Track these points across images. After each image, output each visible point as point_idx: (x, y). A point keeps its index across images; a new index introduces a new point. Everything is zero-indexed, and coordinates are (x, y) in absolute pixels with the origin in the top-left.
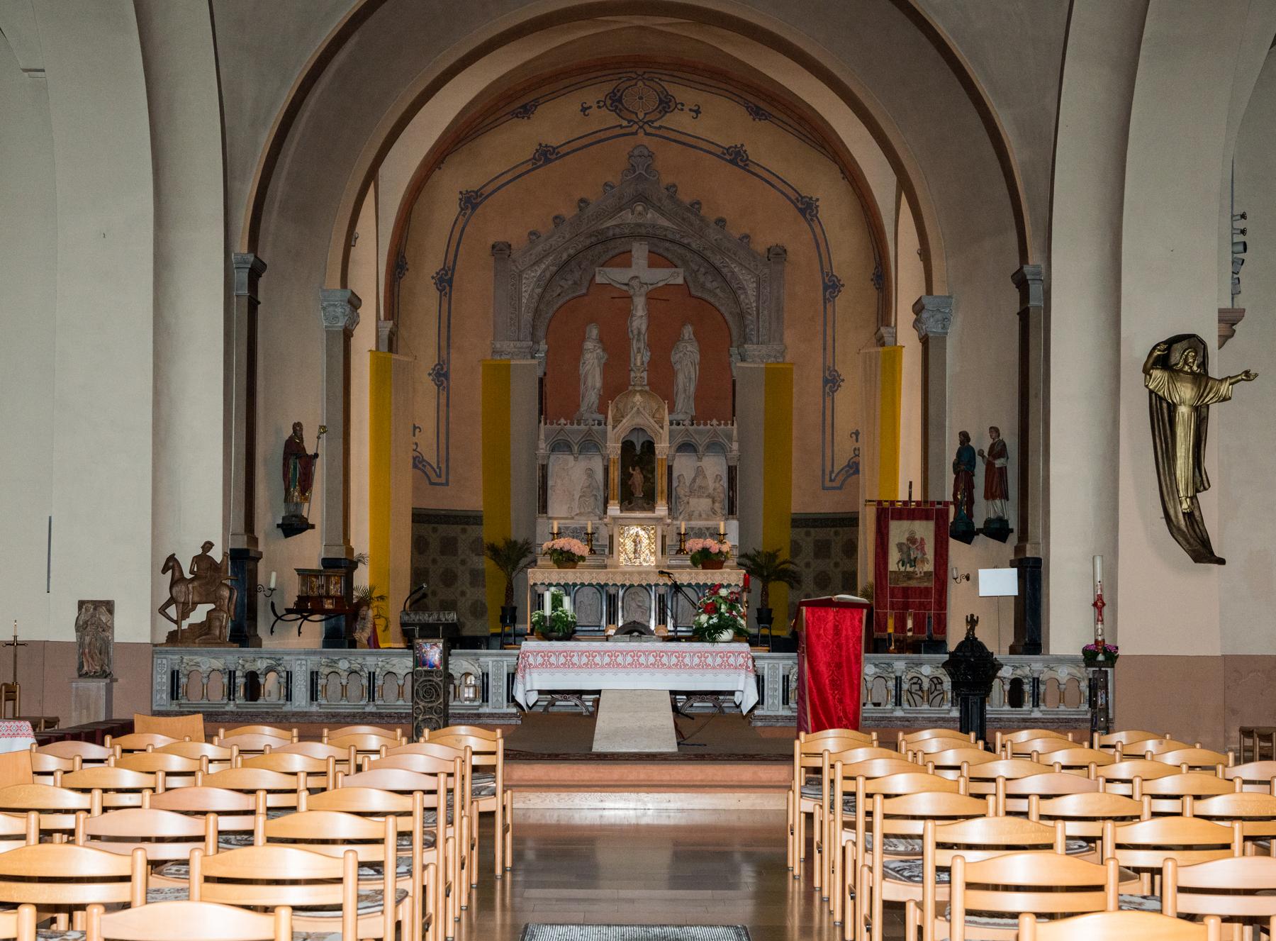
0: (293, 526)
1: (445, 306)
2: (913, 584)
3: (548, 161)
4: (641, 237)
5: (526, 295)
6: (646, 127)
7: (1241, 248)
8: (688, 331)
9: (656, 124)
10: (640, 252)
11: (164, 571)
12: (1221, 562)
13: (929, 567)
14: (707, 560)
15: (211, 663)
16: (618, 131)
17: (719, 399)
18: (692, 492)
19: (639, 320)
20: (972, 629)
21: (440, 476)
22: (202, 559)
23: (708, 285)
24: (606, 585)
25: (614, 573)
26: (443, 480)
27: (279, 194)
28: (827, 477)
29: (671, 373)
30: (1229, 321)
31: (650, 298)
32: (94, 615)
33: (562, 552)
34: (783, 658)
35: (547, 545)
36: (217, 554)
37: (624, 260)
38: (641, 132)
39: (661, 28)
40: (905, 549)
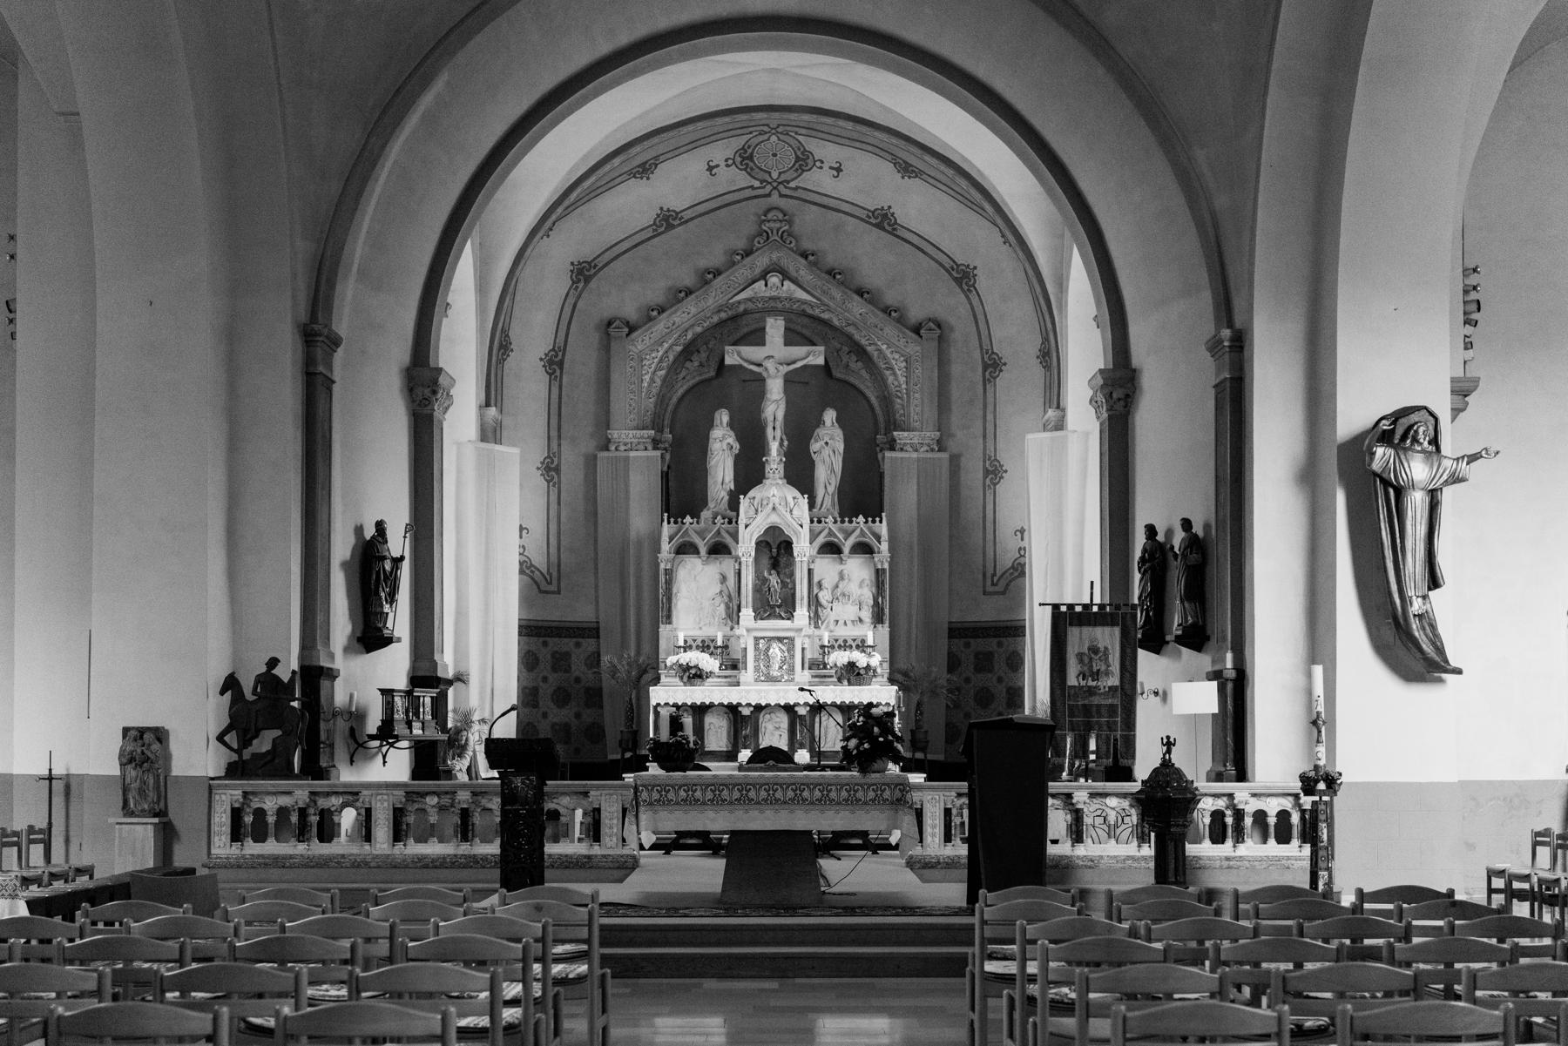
0: (371, 637)
1: (555, 391)
2: (1096, 700)
3: (670, 227)
4: (774, 312)
5: (647, 378)
6: (781, 187)
7: (1474, 307)
8: (830, 416)
9: (792, 185)
10: (775, 329)
11: (222, 693)
12: (1459, 672)
13: (1114, 681)
14: (852, 674)
15: (274, 797)
16: (748, 193)
17: (862, 495)
18: (835, 599)
19: (775, 407)
20: (1169, 751)
21: (550, 583)
22: (268, 681)
23: (853, 365)
24: (739, 705)
25: (748, 692)
26: (553, 588)
27: (357, 255)
28: (989, 582)
29: (810, 466)
30: (1462, 391)
31: (789, 380)
32: (145, 748)
33: (688, 668)
34: (945, 789)
35: (671, 660)
36: (283, 673)
37: (757, 337)
38: (775, 195)
39: (798, 71)
40: (1086, 660)
